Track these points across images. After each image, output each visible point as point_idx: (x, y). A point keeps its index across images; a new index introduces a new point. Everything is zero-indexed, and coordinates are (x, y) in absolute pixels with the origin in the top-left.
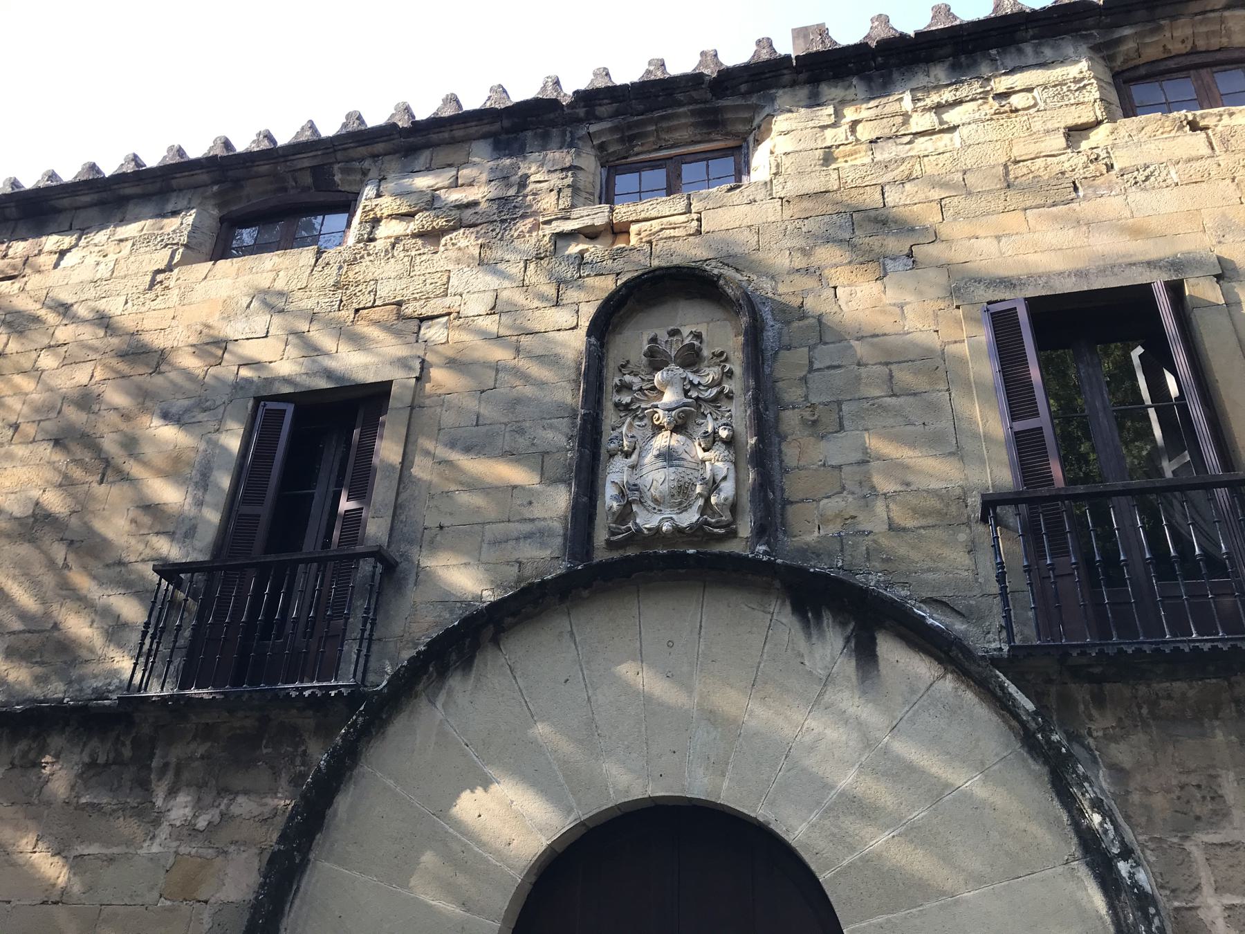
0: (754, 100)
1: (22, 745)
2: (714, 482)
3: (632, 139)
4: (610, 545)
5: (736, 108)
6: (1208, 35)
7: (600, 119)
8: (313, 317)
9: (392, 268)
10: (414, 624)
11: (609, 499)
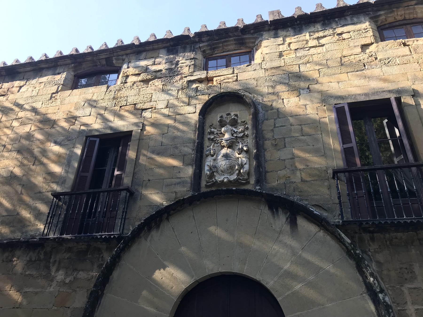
0: (255, 35)
1: (6, 254)
2: (242, 165)
3: (214, 49)
4: (207, 186)
5: (249, 38)
6: (409, 14)
7: (203, 42)
8: (106, 109)
9: (133, 92)
10: (140, 214)
11: (206, 170)
